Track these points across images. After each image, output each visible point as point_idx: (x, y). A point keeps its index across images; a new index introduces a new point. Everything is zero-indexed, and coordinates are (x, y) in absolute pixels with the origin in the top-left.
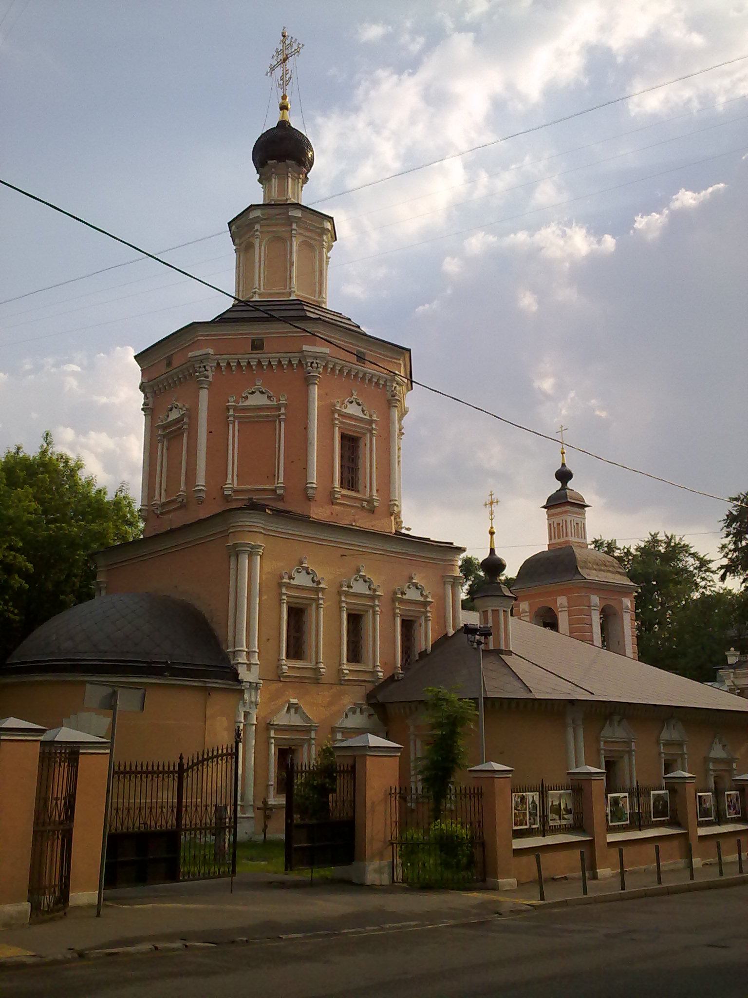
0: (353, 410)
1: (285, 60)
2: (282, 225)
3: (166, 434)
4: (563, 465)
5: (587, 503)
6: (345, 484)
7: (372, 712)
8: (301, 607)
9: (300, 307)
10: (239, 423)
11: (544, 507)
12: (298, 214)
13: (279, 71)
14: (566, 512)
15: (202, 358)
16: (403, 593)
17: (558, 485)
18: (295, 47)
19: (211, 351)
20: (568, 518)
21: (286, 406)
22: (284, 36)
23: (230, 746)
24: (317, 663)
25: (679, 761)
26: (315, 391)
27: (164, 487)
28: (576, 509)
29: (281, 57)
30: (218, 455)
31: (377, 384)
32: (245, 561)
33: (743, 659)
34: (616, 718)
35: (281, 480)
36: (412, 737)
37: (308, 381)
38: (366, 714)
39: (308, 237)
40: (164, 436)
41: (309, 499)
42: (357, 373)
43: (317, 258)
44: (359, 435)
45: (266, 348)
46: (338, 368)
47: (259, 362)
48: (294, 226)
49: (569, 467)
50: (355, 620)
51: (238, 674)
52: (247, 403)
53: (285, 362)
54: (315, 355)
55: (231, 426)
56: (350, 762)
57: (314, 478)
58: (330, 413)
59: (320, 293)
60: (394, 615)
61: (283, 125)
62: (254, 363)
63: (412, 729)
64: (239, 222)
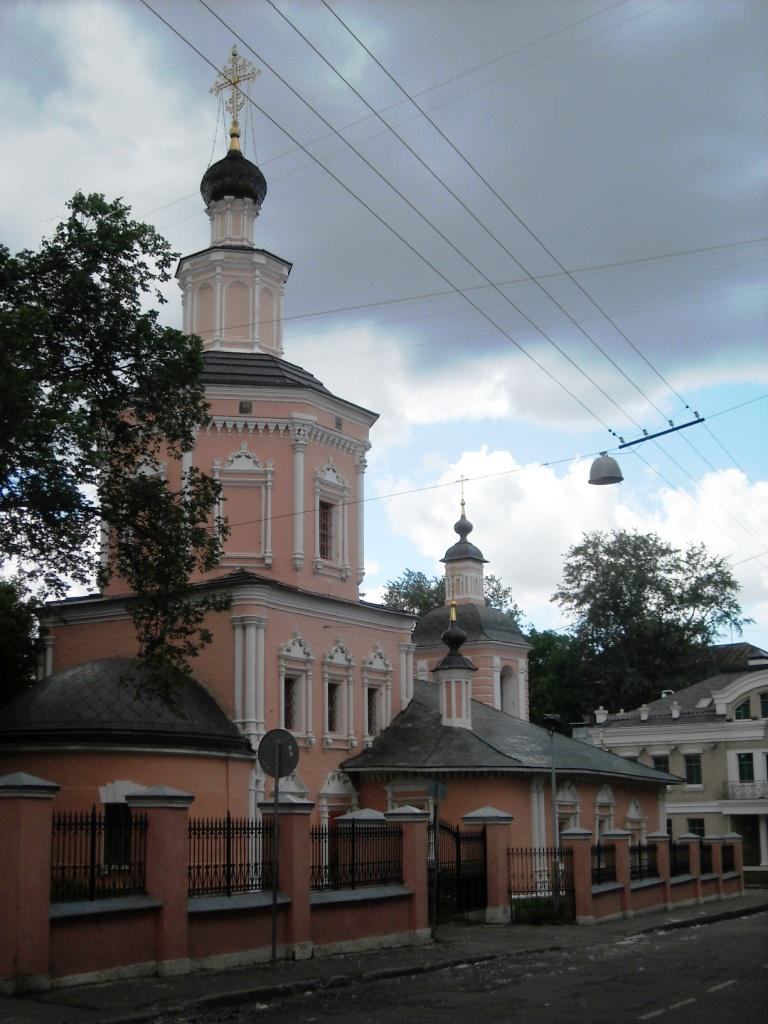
0: (330, 477)
2: (246, 270)
4: (463, 517)
5: (485, 558)
7: (347, 778)
9: (272, 364)
11: (442, 561)
12: (259, 259)
16: (371, 663)
17: (457, 538)
18: (249, 70)
21: (273, 473)
22: (235, 55)
25: (572, 820)
26: (300, 458)
31: (348, 449)
33: (612, 718)
34: (567, 784)
36: (389, 802)
38: (342, 781)
39: (271, 285)
41: (296, 569)
43: (275, 305)
44: (332, 502)
46: (320, 435)
48: (258, 273)
49: (469, 518)
51: (251, 745)
53: (272, 427)
54: (303, 422)
56: (480, 829)
57: (299, 549)
58: (313, 479)
59: (278, 344)
61: (234, 156)
62: (240, 426)
63: (390, 795)
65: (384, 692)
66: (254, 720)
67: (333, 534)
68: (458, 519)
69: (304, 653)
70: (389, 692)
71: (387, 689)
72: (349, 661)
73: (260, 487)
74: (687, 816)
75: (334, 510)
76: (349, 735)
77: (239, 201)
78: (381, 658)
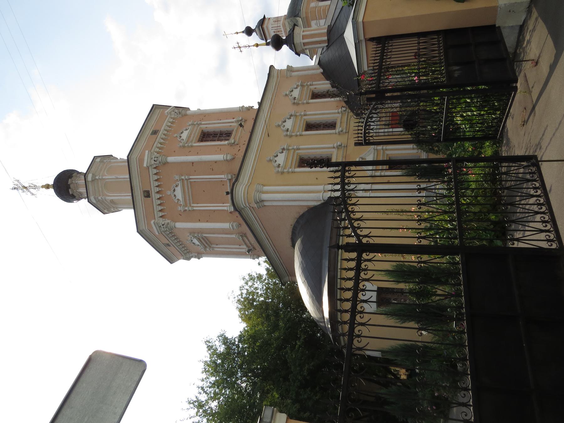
1: (26, 188)
3: (206, 246)
4: (243, 32)
6: (227, 138)
8: (298, 160)
10: (193, 203)
13: (32, 190)
14: (267, 27)
15: (158, 227)
18: (16, 183)
19: (152, 222)
20: (270, 26)
23: (332, 175)
24: (334, 147)
26: (170, 159)
27: (238, 246)
28: (266, 22)
29: (25, 190)
30: (210, 216)
32: (264, 196)
35: (223, 176)
37: (166, 163)
40: (210, 247)
42: (164, 134)
45: (147, 189)
47: (158, 192)
48: (97, 177)
49: (244, 29)
50: (310, 127)
52: (181, 199)
55: (195, 208)
57: (220, 157)
58: (186, 149)
60: (308, 103)
64: (102, 209)
65: (315, 87)
66: (321, 194)
67: (219, 130)
68: (244, 35)
69: (282, 152)
70: (314, 83)
71: (312, 85)
72: (298, 86)
73: (190, 182)
74: (312, 28)
75: (206, 130)
76: (338, 113)
77: (71, 186)
78: (285, 121)
